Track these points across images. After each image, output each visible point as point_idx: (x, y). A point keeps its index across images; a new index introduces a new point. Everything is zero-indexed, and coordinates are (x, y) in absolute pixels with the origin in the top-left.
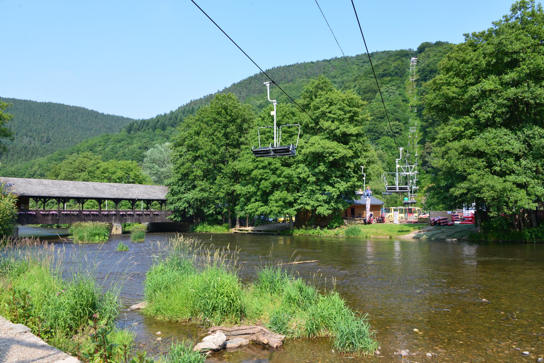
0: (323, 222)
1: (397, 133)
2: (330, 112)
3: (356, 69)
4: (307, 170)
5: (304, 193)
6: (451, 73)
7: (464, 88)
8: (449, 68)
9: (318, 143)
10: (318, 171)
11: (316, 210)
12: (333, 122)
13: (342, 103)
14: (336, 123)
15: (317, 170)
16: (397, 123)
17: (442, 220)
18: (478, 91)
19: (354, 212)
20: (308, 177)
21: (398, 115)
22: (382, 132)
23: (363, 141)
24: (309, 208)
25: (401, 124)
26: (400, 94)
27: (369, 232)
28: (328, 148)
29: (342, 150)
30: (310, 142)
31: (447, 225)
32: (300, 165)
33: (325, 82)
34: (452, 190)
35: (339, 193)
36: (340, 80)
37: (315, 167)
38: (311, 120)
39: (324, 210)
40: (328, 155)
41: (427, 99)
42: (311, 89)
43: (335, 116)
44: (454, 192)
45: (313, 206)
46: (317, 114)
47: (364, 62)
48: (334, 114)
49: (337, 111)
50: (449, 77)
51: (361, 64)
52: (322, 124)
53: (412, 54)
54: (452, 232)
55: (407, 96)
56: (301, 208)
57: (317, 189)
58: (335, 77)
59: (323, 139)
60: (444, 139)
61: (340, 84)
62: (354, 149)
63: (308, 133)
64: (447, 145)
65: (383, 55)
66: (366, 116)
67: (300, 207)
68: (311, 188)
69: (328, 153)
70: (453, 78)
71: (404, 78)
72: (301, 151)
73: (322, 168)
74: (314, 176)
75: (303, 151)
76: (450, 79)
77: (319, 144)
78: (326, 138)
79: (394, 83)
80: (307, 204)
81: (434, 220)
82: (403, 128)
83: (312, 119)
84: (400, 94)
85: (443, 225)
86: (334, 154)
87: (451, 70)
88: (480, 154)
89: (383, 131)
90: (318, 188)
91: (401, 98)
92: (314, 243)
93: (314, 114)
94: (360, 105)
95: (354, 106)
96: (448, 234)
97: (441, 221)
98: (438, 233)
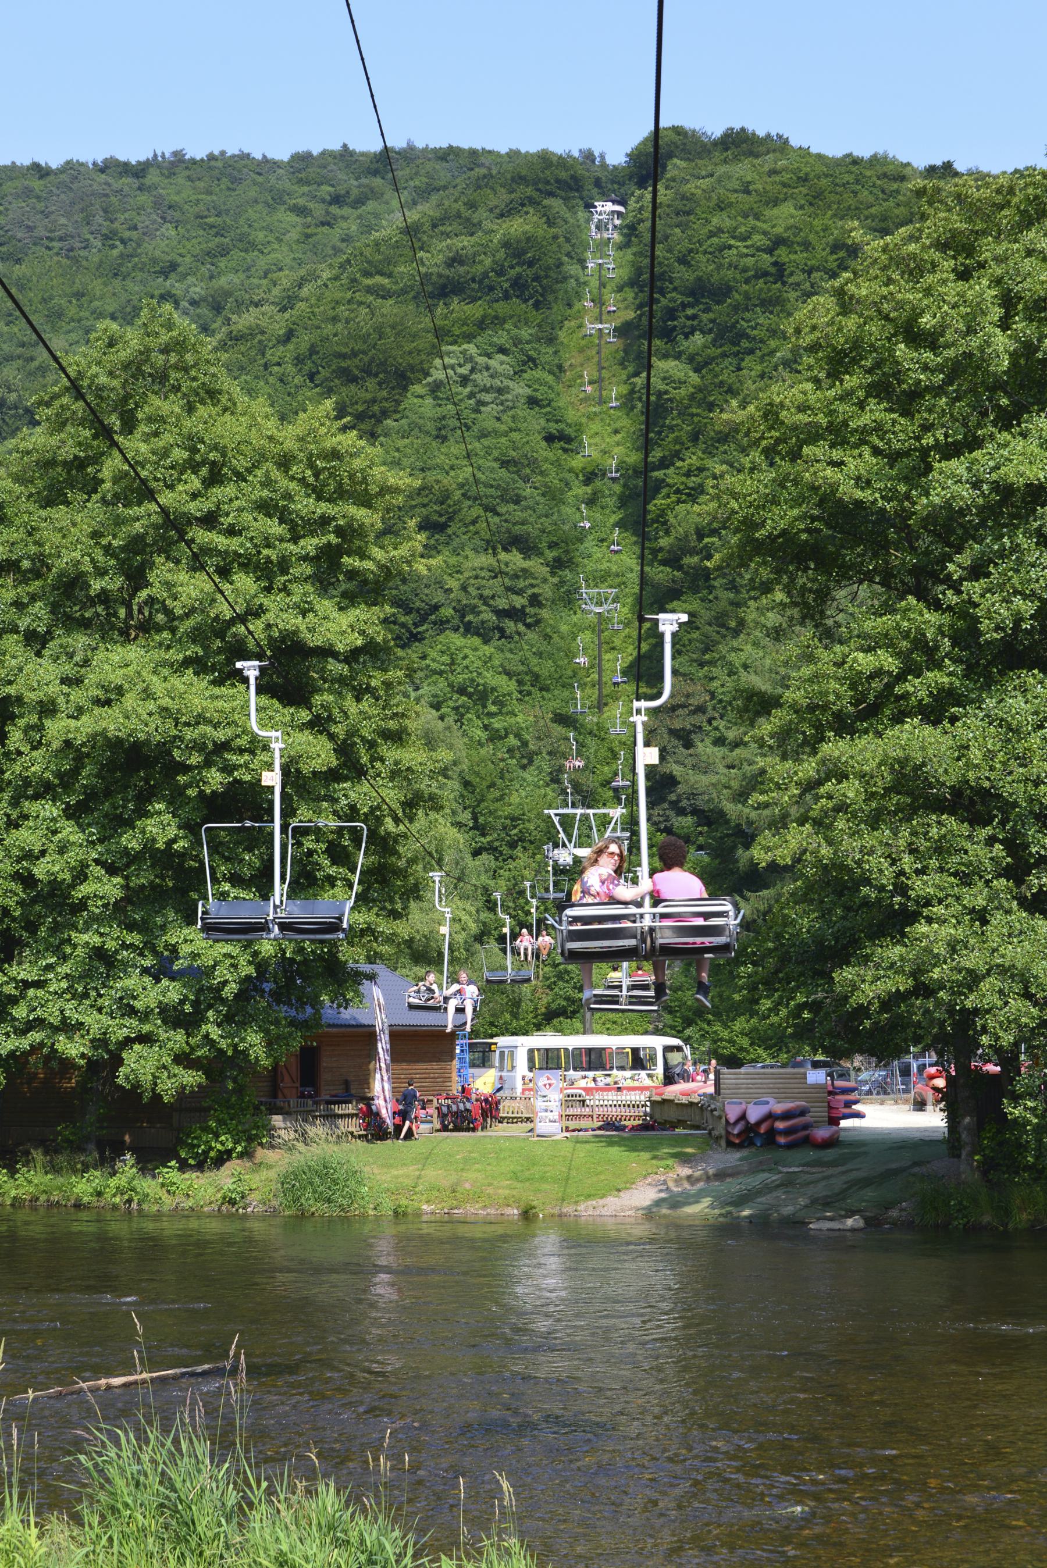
0: (157, 1131)
1: (513, 614)
2: (209, 520)
3: (294, 235)
4: (78, 837)
5: (49, 968)
6: (851, 381)
7: (917, 467)
8: (844, 354)
9: (138, 688)
10: (134, 845)
11: (120, 1062)
12: (224, 572)
13: (276, 474)
14: (245, 582)
15: (130, 841)
16: (515, 559)
17: (786, 1116)
18: (976, 485)
19: (319, 1073)
20: (81, 875)
21: (520, 515)
22: (436, 608)
23: (388, 685)
24: (73, 1048)
25: (536, 565)
26: (533, 402)
27: (407, 1178)
28: (200, 719)
29: (276, 742)
30: (91, 678)
31: (808, 1142)
32: (32, 807)
33: (179, 346)
34: (846, 974)
35: (251, 970)
36: (198, 290)
37: (121, 823)
38: (99, 555)
39: (151, 1067)
40: (195, 759)
41: (735, 496)
42: (103, 380)
43: (233, 544)
44: (855, 988)
45: (100, 1042)
46: (138, 527)
47: (337, 200)
48: (231, 532)
49: (247, 517)
50: (841, 398)
51: (318, 210)
52: (168, 585)
53: (598, 183)
54: (838, 1184)
55: (571, 415)
56: (35, 1049)
57: (125, 946)
58: (173, 266)
59: (164, 663)
60: (812, 708)
61: (204, 311)
62: (339, 730)
63: (85, 624)
64: (827, 749)
65: (443, 173)
66: (403, 551)
67: (25, 1043)
68: (96, 940)
69: (198, 746)
70: (861, 405)
71: (558, 309)
72: (40, 728)
73: (160, 826)
74: (112, 870)
75: (56, 728)
76: (842, 408)
77: (147, 694)
78: (187, 662)
79: (502, 338)
80: (68, 1028)
81: (743, 1117)
82: (546, 591)
83: (108, 550)
84: (533, 402)
85: (790, 1146)
86: (233, 758)
87: (854, 361)
88: (974, 804)
89: (439, 597)
90: (134, 938)
91: (536, 422)
92: (105, 1246)
93: (119, 521)
94: (374, 489)
95: (341, 494)
96: (820, 1190)
97: (780, 1125)
98: (767, 1189)
